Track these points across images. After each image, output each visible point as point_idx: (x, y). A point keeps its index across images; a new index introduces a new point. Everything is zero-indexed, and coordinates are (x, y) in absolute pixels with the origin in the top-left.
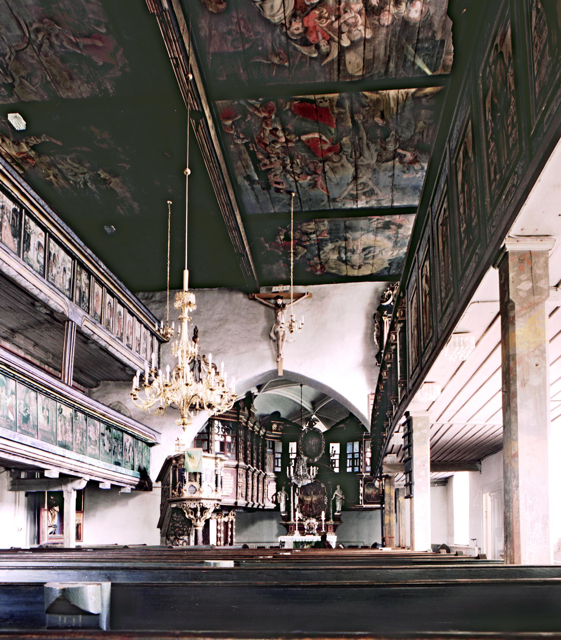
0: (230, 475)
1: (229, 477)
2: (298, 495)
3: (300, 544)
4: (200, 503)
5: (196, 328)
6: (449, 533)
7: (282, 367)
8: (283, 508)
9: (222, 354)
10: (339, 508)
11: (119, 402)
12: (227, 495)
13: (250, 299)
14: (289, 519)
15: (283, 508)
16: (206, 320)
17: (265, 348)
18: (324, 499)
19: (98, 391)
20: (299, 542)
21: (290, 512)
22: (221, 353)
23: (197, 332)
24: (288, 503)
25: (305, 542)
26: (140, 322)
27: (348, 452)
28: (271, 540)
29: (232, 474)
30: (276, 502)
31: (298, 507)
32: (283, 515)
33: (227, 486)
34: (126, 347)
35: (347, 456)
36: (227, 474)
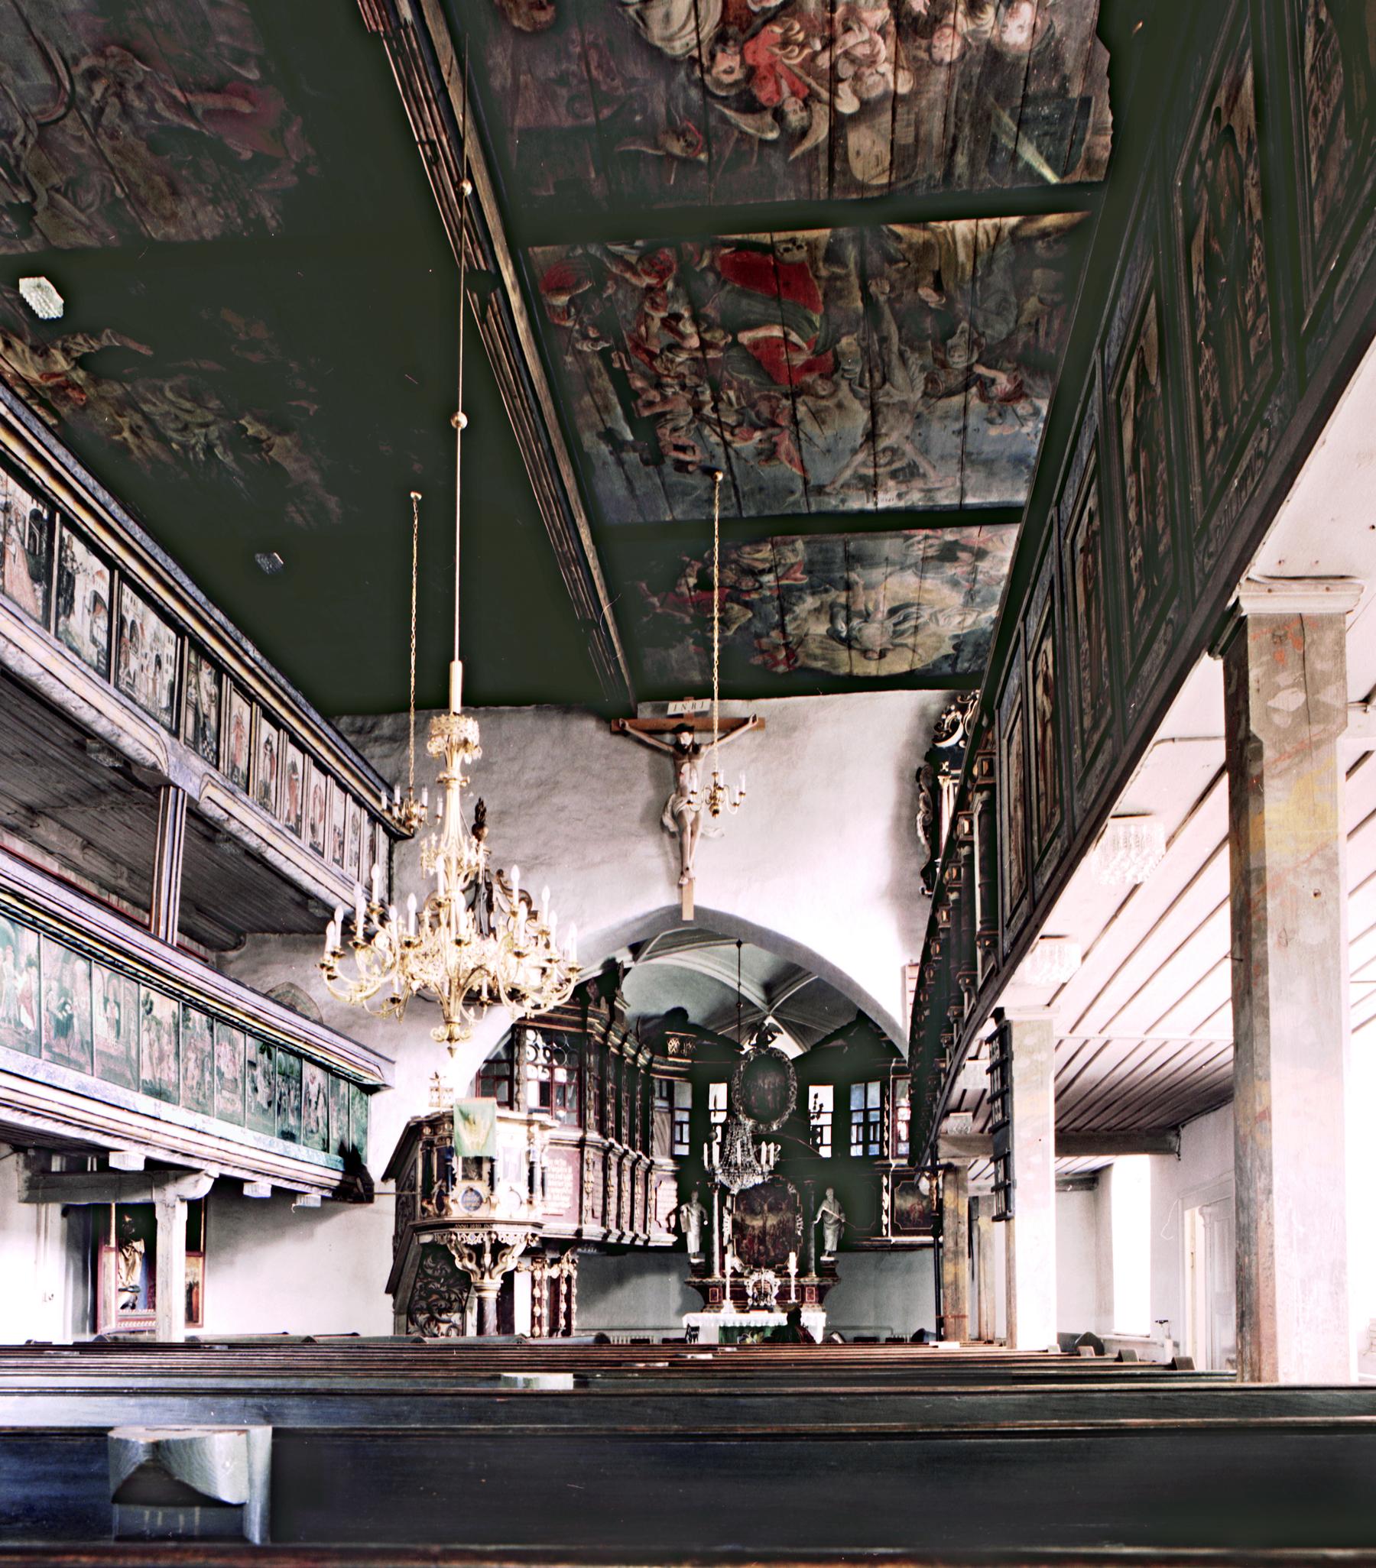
0: (564, 1163)
1: (561, 1170)
2: (730, 1212)
3: (736, 1333)
4: (490, 1233)
5: (481, 803)
6: (1100, 1307)
7: (691, 899)
8: (693, 1244)
9: (543, 868)
10: (830, 1244)
11: (291, 985)
12: (556, 1212)
13: (614, 733)
14: (709, 1272)
15: (693, 1244)
16: (506, 784)
17: (650, 853)
18: (795, 1222)
19: (240, 957)
20: (733, 1328)
21: (712, 1254)
22: (542, 864)
23: (483, 814)
24: (705, 1233)
25: (748, 1328)
26: (344, 788)
27: (853, 1108)
28: (666, 1324)
29: (569, 1162)
30: (677, 1230)
31: (730, 1241)
32: (695, 1261)
33: (558, 1190)
34: (310, 851)
35: (850, 1118)
36: (557, 1162)
